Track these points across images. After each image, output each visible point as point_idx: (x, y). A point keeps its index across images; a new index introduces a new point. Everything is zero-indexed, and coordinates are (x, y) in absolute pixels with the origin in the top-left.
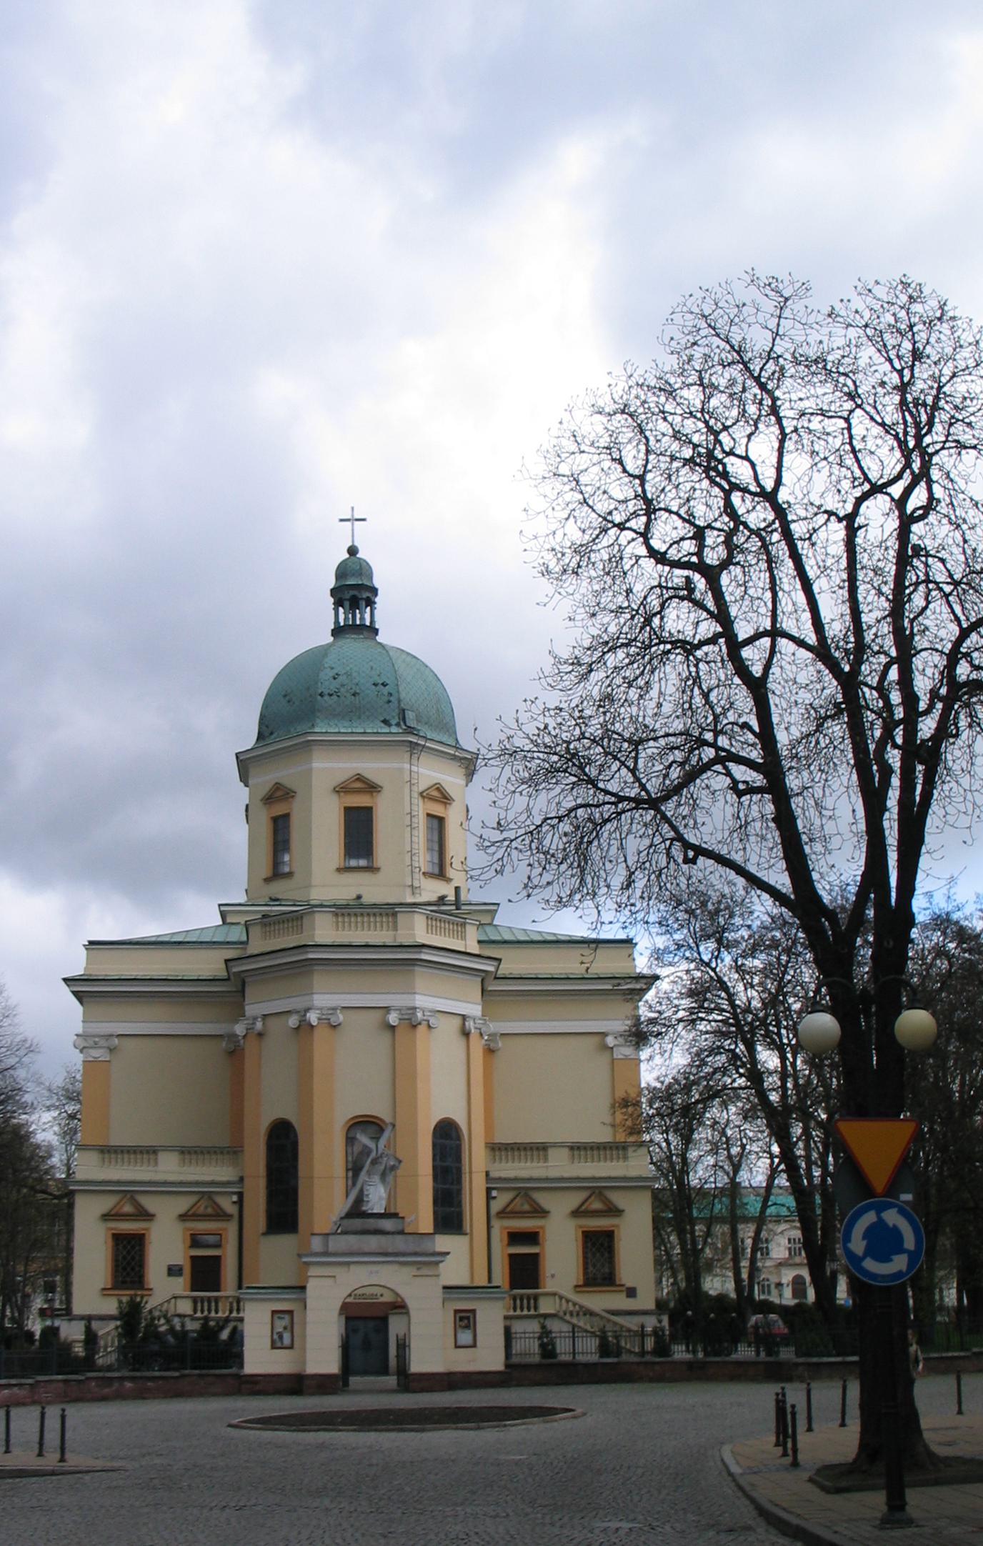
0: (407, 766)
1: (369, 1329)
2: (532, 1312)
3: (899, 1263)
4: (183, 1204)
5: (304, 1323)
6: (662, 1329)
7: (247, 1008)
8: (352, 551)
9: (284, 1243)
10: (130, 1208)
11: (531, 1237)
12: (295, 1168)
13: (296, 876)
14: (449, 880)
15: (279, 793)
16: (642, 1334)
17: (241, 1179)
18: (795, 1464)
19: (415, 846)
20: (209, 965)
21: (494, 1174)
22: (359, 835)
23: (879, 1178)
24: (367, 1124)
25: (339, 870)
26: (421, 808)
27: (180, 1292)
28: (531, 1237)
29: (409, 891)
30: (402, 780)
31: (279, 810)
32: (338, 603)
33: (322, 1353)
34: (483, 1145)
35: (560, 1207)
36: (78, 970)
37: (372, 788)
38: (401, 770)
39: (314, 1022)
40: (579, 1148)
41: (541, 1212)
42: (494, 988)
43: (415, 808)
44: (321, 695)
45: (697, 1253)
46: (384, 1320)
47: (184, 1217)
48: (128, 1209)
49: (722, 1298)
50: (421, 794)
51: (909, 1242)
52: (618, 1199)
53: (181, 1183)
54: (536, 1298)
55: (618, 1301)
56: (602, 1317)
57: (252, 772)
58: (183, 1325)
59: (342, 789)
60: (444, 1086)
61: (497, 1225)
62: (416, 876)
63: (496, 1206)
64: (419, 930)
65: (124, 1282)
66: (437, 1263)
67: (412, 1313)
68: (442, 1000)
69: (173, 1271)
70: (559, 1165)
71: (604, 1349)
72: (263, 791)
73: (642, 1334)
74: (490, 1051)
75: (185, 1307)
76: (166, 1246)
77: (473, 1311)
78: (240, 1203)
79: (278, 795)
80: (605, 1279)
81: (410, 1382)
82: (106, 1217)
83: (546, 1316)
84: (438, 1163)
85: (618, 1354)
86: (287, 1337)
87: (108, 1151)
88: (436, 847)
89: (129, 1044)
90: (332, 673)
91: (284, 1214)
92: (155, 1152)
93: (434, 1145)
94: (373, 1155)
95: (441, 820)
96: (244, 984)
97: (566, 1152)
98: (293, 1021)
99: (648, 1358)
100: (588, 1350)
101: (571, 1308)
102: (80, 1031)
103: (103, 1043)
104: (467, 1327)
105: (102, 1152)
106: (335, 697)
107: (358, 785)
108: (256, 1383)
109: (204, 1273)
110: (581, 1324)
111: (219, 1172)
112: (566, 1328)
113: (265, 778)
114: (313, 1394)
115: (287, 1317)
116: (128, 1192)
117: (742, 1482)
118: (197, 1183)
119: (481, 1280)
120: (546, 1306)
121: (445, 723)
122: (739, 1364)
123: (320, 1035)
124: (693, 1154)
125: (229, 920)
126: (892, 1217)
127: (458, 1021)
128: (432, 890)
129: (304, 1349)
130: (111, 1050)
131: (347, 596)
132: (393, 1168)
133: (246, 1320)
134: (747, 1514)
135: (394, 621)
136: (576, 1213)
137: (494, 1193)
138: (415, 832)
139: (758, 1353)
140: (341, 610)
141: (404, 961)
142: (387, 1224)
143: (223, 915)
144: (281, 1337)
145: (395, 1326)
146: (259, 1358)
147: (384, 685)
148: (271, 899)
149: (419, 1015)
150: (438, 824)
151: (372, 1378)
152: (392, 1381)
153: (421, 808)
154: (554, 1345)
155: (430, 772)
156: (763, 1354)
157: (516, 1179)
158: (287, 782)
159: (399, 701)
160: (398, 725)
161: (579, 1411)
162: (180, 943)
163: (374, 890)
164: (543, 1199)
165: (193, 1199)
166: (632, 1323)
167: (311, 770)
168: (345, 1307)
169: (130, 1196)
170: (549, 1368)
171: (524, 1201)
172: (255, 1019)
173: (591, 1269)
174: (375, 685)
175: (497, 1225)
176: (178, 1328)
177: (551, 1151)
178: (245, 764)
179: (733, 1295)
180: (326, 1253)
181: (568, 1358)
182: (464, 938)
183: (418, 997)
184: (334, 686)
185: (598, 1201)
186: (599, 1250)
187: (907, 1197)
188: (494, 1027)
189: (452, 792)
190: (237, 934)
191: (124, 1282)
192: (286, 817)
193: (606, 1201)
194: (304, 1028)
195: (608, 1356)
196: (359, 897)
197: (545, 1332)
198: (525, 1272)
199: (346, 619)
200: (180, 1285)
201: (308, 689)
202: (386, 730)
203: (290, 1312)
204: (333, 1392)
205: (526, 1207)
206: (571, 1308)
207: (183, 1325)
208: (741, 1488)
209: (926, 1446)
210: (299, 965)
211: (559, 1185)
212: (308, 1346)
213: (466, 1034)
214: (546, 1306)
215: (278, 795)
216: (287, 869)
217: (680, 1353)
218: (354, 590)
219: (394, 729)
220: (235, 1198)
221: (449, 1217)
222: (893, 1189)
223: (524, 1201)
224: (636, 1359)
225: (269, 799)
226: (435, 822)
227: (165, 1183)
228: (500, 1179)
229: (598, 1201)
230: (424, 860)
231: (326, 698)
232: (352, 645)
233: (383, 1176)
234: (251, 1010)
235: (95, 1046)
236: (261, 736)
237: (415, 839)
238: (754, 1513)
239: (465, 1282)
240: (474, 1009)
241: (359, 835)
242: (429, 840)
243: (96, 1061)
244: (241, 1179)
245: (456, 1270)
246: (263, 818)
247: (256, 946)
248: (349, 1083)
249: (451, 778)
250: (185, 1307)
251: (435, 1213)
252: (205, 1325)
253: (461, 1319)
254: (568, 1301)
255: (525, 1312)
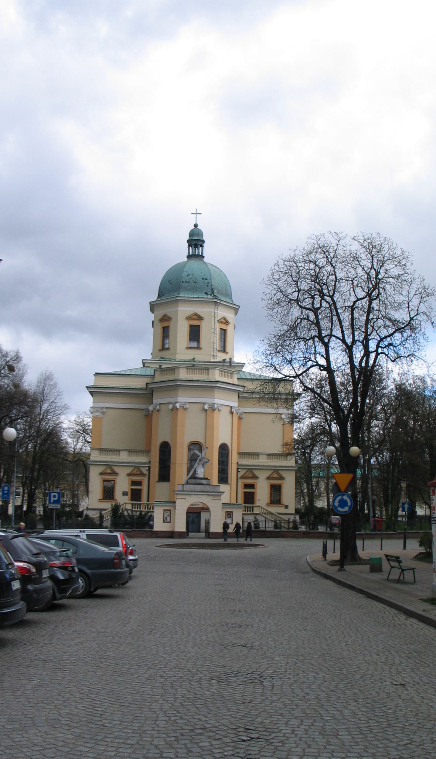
0: (213, 310)
1: (194, 516)
2: (251, 512)
3: (346, 509)
4: (129, 470)
5: (175, 514)
6: (296, 521)
7: (154, 401)
8: (196, 226)
9: (165, 484)
10: (110, 471)
11: (252, 486)
12: (170, 459)
13: (171, 350)
14: (227, 353)
15: (165, 318)
16: (289, 522)
17: (150, 462)
18: (325, 560)
19: (215, 340)
20: (140, 383)
21: (240, 463)
22: (195, 333)
23: (343, 488)
24: (196, 446)
25: (187, 348)
26: (218, 326)
27: (127, 501)
28: (252, 486)
29: (212, 357)
30: (211, 316)
31: (165, 324)
32: (190, 245)
33: (180, 526)
34: (236, 453)
35: (262, 476)
36: (91, 384)
37: (200, 318)
38: (211, 312)
39: (178, 407)
40: (270, 455)
41: (256, 477)
42: (244, 396)
43: (216, 326)
44: (183, 282)
45: (313, 491)
46: (199, 514)
47: (129, 475)
48: (109, 471)
49: (322, 509)
50: (218, 321)
51: (349, 504)
52: (283, 474)
53: (128, 463)
54: (253, 507)
55: (282, 510)
56: (276, 515)
57: (156, 309)
58: (132, 514)
59: (189, 318)
60: (223, 432)
61: (240, 481)
62: (215, 351)
63: (240, 475)
64: (216, 375)
65: (107, 497)
66: (220, 495)
67: (212, 512)
68: (224, 401)
69: (125, 494)
70: (263, 461)
71: (276, 526)
72: (160, 317)
73: (289, 522)
74: (240, 418)
75: (129, 507)
76: (122, 485)
77: (232, 512)
78: (149, 470)
79: (165, 319)
80: (277, 501)
81: (209, 535)
82: (101, 474)
83: (256, 514)
84: (220, 459)
85: (280, 528)
86: (168, 518)
87: (102, 450)
88: (223, 341)
89: (109, 410)
90: (187, 274)
91: (165, 474)
92: (119, 451)
93: (219, 452)
94: (200, 458)
95: (225, 331)
96: (153, 391)
97: (265, 456)
98: (171, 406)
99: (291, 530)
100: (270, 527)
101: (265, 511)
102: (92, 406)
103: (100, 410)
104: (230, 517)
105: (100, 450)
106: (187, 283)
107: (195, 317)
108: (157, 534)
109: (136, 495)
110: (268, 517)
111: (142, 459)
112: (263, 519)
113: (161, 312)
114: (176, 538)
115: (169, 512)
116: (109, 465)
117: (310, 564)
118: (134, 463)
119: (234, 502)
120: (256, 511)
121: (228, 294)
122: (320, 533)
123: (180, 413)
124: (313, 456)
125: (146, 365)
126: (345, 497)
127: (229, 408)
128: (220, 357)
129: (174, 523)
130: (103, 413)
131: (193, 243)
132: (206, 462)
133: (155, 512)
134: (309, 569)
135: (209, 251)
136: (268, 478)
137: (239, 470)
138: (215, 335)
139: (327, 529)
140: (191, 248)
141: (211, 387)
142: (204, 482)
143: (144, 364)
144: (166, 519)
145: (204, 516)
146: (159, 525)
147: (206, 279)
148: (162, 358)
149: (216, 406)
150: (224, 332)
151: (195, 534)
152: (203, 535)
153: (218, 326)
154: (259, 524)
155: (222, 312)
156: (328, 530)
157: (247, 465)
158: (169, 315)
159: (211, 286)
160: (211, 295)
161: (266, 545)
162: (129, 375)
163: (200, 356)
164: (257, 473)
165: (132, 469)
166: (286, 518)
167: (177, 311)
168: (189, 508)
169: (110, 467)
170: (250, 532)
171: (250, 473)
172: (157, 405)
173: (272, 498)
174: (203, 279)
175: (240, 481)
176: (131, 514)
177: (260, 456)
178: (153, 307)
179: (326, 507)
180: (183, 491)
181: (263, 529)
182: (232, 378)
183: (215, 399)
184: (187, 279)
185: (276, 474)
186: (276, 492)
187: (350, 493)
188: (242, 410)
189: (229, 320)
190: (150, 372)
191: (107, 497)
192: (168, 327)
193: (279, 474)
194: (175, 409)
195: (277, 529)
196: (194, 359)
197: (256, 520)
198: (249, 498)
199: (192, 252)
200: (127, 499)
201: (178, 279)
202: (206, 296)
203: (170, 510)
204: (184, 538)
205: (251, 475)
206: (265, 511)
207: (132, 514)
208: (309, 565)
209: (358, 556)
210: (173, 386)
211: (262, 468)
212: (176, 521)
213: (232, 413)
214: (256, 511)
215: (165, 319)
216: (167, 346)
217: (303, 528)
218: (196, 241)
219: (209, 297)
220: (147, 468)
221: (223, 478)
222: (346, 491)
223: (250, 473)
224: (287, 530)
225: (162, 320)
226: (223, 331)
227: (123, 463)
228: (242, 465)
229: (276, 474)
230: (218, 346)
231: (184, 283)
232: (194, 263)
233: (203, 465)
234: (155, 401)
235: (97, 411)
236: (159, 296)
237: (215, 338)
238: (310, 569)
239: (228, 502)
240: (235, 404)
241: (195, 333)
242: (220, 338)
243: (97, 417)
244: (150, 462)
245: (225, 498)
246: (159, 327)
247: (158, 378)
248: (190, 430)
249: (229, 315)
250: (129, 507)
251: (218, 476)
252: (141, 514)
253: (228, 514)
254: (264, 509)
255: (249, 512)
